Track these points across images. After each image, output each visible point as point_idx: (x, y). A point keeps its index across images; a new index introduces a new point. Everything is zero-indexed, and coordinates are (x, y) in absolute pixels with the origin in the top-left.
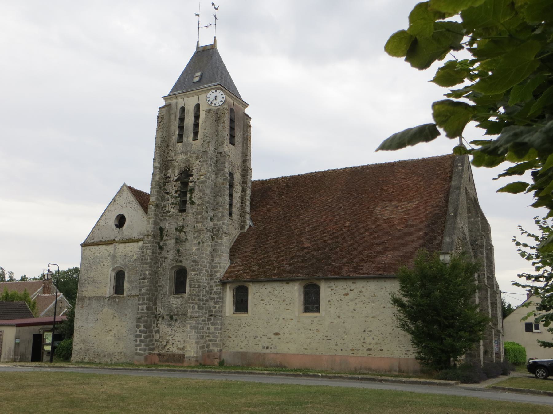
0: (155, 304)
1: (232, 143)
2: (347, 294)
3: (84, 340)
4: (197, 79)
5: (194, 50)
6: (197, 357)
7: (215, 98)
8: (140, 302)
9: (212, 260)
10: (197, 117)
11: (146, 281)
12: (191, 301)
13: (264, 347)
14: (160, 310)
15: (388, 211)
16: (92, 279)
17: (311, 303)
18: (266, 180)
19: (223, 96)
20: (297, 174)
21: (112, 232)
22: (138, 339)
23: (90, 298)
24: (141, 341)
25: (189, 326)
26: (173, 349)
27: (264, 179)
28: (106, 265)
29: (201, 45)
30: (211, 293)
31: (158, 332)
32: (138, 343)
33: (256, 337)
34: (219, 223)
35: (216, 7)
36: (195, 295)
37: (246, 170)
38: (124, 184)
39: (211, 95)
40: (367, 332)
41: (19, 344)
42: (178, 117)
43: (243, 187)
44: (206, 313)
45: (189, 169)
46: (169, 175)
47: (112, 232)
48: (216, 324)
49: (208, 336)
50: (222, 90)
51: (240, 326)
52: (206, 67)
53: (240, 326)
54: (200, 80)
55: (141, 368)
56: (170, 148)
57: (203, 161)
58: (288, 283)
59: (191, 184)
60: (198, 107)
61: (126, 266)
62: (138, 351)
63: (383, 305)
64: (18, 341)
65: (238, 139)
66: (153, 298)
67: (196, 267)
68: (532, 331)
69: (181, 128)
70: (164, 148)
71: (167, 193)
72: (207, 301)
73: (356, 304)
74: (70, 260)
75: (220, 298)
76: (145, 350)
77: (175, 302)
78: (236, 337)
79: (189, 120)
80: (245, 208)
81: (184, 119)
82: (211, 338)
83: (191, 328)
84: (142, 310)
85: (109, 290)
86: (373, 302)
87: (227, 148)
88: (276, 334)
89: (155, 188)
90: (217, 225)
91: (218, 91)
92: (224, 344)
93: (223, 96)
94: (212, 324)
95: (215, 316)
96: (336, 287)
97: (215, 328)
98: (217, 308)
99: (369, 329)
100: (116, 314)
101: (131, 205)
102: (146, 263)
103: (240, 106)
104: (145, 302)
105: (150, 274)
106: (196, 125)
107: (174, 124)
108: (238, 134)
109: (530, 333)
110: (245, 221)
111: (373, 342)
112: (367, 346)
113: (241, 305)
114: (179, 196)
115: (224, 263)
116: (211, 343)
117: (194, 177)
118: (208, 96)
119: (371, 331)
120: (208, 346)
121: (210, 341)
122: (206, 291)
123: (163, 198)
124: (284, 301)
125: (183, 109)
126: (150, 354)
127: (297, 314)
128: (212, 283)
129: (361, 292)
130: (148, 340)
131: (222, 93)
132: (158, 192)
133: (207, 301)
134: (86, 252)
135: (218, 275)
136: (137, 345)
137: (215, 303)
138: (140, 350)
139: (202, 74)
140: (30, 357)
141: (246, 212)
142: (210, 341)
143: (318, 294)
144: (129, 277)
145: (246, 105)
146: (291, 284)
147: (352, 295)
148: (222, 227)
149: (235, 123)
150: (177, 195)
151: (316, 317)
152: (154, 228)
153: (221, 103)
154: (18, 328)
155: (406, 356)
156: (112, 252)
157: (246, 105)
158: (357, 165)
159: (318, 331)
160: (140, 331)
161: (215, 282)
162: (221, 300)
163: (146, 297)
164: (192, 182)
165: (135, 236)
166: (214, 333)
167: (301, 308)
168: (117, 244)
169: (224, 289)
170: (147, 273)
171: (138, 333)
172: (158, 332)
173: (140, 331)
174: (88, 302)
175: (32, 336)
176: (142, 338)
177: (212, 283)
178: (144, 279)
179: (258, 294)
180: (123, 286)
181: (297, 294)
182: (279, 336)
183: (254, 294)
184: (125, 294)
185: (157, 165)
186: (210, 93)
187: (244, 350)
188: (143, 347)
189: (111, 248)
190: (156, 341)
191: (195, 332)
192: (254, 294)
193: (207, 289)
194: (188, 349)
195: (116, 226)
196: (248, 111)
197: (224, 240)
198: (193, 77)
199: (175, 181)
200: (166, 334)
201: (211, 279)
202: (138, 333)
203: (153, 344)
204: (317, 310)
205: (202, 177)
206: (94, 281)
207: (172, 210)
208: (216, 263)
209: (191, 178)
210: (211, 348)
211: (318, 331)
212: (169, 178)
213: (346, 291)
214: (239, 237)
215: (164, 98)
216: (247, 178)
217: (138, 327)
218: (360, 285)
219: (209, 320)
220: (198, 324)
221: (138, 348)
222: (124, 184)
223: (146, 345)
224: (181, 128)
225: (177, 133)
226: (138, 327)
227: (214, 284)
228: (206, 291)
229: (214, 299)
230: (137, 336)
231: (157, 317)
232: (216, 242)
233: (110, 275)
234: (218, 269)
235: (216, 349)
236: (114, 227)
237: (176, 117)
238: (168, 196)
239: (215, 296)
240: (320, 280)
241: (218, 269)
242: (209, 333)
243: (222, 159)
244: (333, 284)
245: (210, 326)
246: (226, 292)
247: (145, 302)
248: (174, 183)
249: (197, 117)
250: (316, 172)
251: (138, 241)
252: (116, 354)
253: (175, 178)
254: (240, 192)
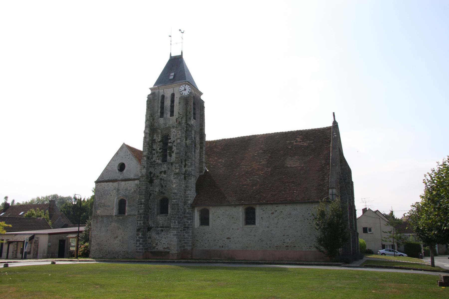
0: (148, 220)
1: (194, 118)
2: (273, 213)
3: (99, 244)
4: (171, 77)
5: (168, 58)
6: (177, 253)
7: (186, 91)
8: (139, 219)
9: (185, 193)
10: (172, 101)
11: (143, 206)
12: (173, 218)
13: (220, 247)
14: (151, 223)
15: (293, 163)
16: (103, 204)
17: (250, 219)
18: (212, 141)
19: (190, 89)
20: (232, 137)
21: (117, 175)
22: (138, 243)
23: (102, 217)
24: (140, 244)
25: (172, 234)
26: (160, 248)
27: (211, 140)
28: (113, 196)
29: (172, 55)
30: (185, 213)
31: (150, 238)
32: (138, 245)
33: (215, 240)
34: (189, 169)
35: (182, 31)
36: (175, 215)
37: (202, 135)
38: (124, 144)
39: (182, 88)
40: (285, 236)
41: (50, 246)
42: (160, 101)
43: (201, 146)
44: (182, 226)
45: (168, 135)
46: (154, 138)
47: (117, 175)
48: (189, 233)
49: (184, 240)
50: (189, 85)
51: (204, 233)
52: (175, 69)
53: (204, 233)
54: (174, 77)
55: (219, 261)
56: (155, 121)
57: (178, 130)
58: (235, 207)
59: (169, 144)
60: (173, 95)
61: (126, 196)
62: (138, 250)
63: (295, 220)
64: (50, 244)
65: (198, 116)
66: (146, 216)
67: (176, 197)
68: (367, 232)
69: (162, 108)
70: (151, 121)
71: (154, 150)
72: (182, 218)
73: (279, 219)
74: (86, 192)
75: (191, 216)
76: (143, 249)
77: (161, 219)
78: (202, 240)
79: (168, 103)
80: (202, 159)
81: (164, 102)
82: (186, 241)
83: (173, 235)
84: (140, 224)
85: (115, 212)
86: (289, 218)
87: (192, 122)
88: (228, 238)
89: (146, 146)
90: (187, 170)
91: (187, 85)
92: (194, 245)
93: (190, 89)
94: (186, 233)
95: (188, 228)
96: (266, 209)
97: (188, 235)
98: (189, 223)
99: (287, 234)
100: (120, 227)
101: (128, 157)
102: (142, 195)
103: (198, 95)
104: (142, 219)
105: (144, 201)
106: (172, 107)
107: (157, 105)
108: (198, 112)
109: (366, 234)
110: (202, 168)
111: (290, 242)
112: (285, 245)
113: (205, 221)
114: (162, 151)
115: (192, 194)
116: (186, 245)
117: (172, 139)
118: (180, 88)
119: (288, 235)
120: (184, 246)
121: (185, 243)
122: (182, 212)
123: (151, 152)
124: (233, 218)
125: (163, 97)
126: (145, 252)
127: (241, 226)
128: (186, 207)
129: (281, 212)
130: (144, 243)
131: (189, 87)
132: (148, 149)
133: (182, 218)
134: (98, 187)
135: (189, 202)
136: (137, 247)
137: (188, 219)
138: (139, 249)
139: (175, 74)
140: (57, 255)
141: (203, 162)
142: (185, 243)
143: (254, 213)
144: (129, 203)
145: (201, 94)
146: (237, 208)
147: (276, 214)
148: (191, 172)
149: (194, 106)
150: (160, 151)
151: (253, 228)
152: (147, 172)
153: (188, 93)
154: (50, 236)
155: (310, 250)
156: (117, 187)
157: (201, 94)
158: (270, 132)
159: (255, 236)
160: (139, 238)
161: (188, 206)
162: (192, 218)
163: (142, 216)
164: (170, 143)
165: (132, 177)
166: (187, 238)
167: (244, 222)
168: (120, 182)
169: (193, 211)
170: (143, 200)
171: (138, 238)
172: (150, 238)
173: (139, 238)
174: (101, 219)
175: (58, 241)
176: (141, 242)
177: (186, 207)
178: (141, 204)
179: (216, 214)
180: (125, 209)
181: (241, 214)
182: (230, 240)
183: (213, 214)
184: (126, 214)
185: (147, 131)
186: (182, 86)
187: (207, 248)
188: (141, 247)
189: (116, 184)
190: (149, 243)
191: (176, 238)
192: (213, 214)
193: (183, 211)
194: (173, 248)
195: (119, 170)
196: (202, 97)
197: (192, 180)
198: (169, 76)
199: (159, 142)
200: (155, 239)
201: (184, 205)
202: (138, 238)
203: (147, 246)
204: (254, 223)
205: (178, 140)
206: (104, 206)
207: (157, 161)
208: (188, 194)
209: (170, 141)
210: (186, 248)
211: (255, 236)
212: (155, 140)
213: (273, 211)
214: (199, 177)
215: (151, 89)
216: (203, 140)
217: (138, 235)
218: (281, 208)
219: (184, 230)
220: (178, 232)
221: (138, 248)
222: (124, 144)
223: (144, 246)
224: (162, 108)
225: (159, 111)
226: (138, 235)
227: (187, 208)
228: (182, 212)
229: (187, 217)
230: (137, 241)
231: (149, 229)
232: (187, 181)
233: (116, 201)
234: (189, 198)
235: (189, 248)
236: (117, 171)
237: (158, 101)
238: (154, 152)
239: (188, 215)
240: (256, 204)
241: (189, 198)
242: (184, 238)
243: (190, 129)
244: (264, 207)
245: (185, 234)
246: (194, 212)
247: (142, 219)
248: (158, 143)
249: (172, 101)
250: (244, 137)
251: (134, 180)
252: (121, 252)
253: (159, 140)
254: (199, 149)
